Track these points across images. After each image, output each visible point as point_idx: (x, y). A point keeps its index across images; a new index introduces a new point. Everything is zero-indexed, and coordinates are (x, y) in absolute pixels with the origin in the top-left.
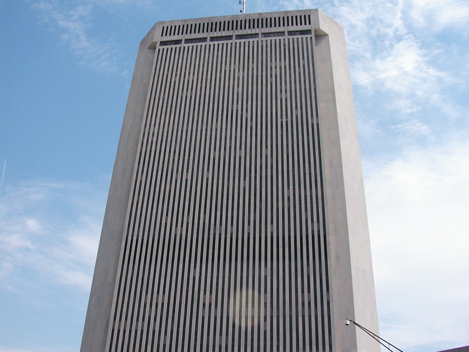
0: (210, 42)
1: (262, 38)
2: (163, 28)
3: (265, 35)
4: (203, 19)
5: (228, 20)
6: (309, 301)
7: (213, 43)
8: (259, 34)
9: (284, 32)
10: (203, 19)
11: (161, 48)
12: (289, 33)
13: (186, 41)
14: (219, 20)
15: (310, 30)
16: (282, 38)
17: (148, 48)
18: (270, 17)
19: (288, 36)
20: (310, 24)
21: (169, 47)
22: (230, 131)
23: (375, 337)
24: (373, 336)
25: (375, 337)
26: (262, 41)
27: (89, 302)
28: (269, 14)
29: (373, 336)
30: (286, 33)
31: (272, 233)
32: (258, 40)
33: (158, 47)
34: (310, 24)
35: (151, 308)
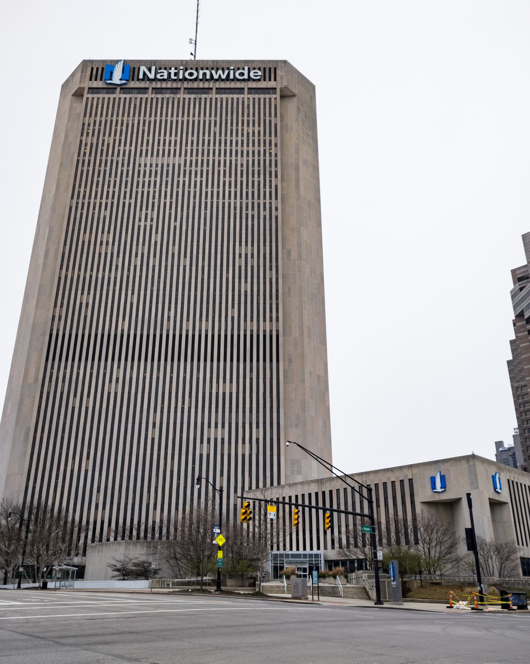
0: (152, 95)
1: (88, 95)
2: (92, 69)
3: (124, 91)
4: (102, 62)
5: (102, 67)
6: (49, 391)
7: (155, 96)
8: (245, 89)
9: (243, 89)
10: (235, 62)
11: (90, 96)
12: (217, 90)
13: (90, 90)
14: (272, 65)
15: (275, 89)
16: (241, 96)
17: (72, 95)
18: (264, 67)
19: (248, 95)
20: (275, 80)
21: (101, 96)
22: (199, 210)
23: (319, 459)
24: (316, 457)
25: (319, 459)
26: (216, 98)
27: (11, 368)
28: (236, 63)
29: (316, 457)
30: (246, 90)
31: (207, 331)
32: (147, 97)
33: (86, 95)
34: (275, 80)
35: (63, 384)
